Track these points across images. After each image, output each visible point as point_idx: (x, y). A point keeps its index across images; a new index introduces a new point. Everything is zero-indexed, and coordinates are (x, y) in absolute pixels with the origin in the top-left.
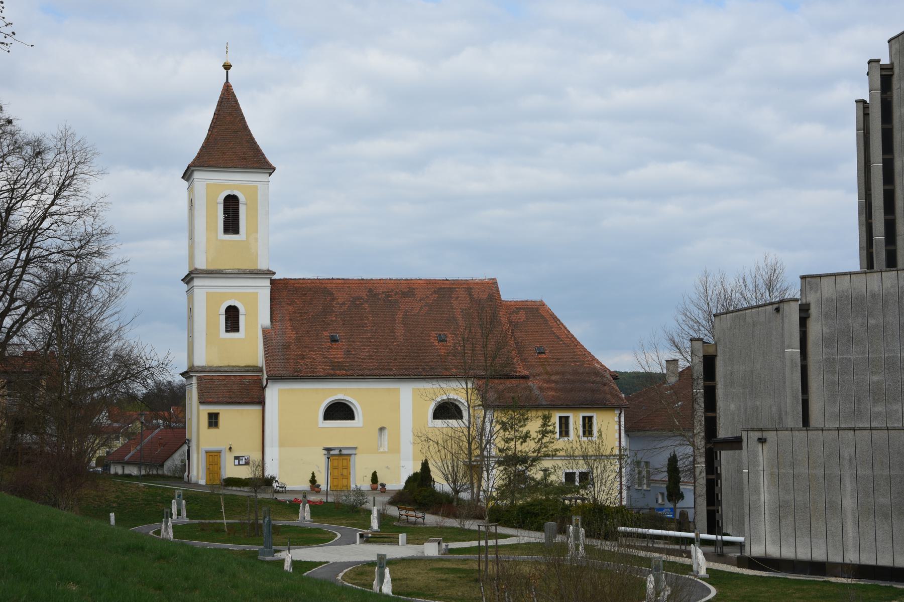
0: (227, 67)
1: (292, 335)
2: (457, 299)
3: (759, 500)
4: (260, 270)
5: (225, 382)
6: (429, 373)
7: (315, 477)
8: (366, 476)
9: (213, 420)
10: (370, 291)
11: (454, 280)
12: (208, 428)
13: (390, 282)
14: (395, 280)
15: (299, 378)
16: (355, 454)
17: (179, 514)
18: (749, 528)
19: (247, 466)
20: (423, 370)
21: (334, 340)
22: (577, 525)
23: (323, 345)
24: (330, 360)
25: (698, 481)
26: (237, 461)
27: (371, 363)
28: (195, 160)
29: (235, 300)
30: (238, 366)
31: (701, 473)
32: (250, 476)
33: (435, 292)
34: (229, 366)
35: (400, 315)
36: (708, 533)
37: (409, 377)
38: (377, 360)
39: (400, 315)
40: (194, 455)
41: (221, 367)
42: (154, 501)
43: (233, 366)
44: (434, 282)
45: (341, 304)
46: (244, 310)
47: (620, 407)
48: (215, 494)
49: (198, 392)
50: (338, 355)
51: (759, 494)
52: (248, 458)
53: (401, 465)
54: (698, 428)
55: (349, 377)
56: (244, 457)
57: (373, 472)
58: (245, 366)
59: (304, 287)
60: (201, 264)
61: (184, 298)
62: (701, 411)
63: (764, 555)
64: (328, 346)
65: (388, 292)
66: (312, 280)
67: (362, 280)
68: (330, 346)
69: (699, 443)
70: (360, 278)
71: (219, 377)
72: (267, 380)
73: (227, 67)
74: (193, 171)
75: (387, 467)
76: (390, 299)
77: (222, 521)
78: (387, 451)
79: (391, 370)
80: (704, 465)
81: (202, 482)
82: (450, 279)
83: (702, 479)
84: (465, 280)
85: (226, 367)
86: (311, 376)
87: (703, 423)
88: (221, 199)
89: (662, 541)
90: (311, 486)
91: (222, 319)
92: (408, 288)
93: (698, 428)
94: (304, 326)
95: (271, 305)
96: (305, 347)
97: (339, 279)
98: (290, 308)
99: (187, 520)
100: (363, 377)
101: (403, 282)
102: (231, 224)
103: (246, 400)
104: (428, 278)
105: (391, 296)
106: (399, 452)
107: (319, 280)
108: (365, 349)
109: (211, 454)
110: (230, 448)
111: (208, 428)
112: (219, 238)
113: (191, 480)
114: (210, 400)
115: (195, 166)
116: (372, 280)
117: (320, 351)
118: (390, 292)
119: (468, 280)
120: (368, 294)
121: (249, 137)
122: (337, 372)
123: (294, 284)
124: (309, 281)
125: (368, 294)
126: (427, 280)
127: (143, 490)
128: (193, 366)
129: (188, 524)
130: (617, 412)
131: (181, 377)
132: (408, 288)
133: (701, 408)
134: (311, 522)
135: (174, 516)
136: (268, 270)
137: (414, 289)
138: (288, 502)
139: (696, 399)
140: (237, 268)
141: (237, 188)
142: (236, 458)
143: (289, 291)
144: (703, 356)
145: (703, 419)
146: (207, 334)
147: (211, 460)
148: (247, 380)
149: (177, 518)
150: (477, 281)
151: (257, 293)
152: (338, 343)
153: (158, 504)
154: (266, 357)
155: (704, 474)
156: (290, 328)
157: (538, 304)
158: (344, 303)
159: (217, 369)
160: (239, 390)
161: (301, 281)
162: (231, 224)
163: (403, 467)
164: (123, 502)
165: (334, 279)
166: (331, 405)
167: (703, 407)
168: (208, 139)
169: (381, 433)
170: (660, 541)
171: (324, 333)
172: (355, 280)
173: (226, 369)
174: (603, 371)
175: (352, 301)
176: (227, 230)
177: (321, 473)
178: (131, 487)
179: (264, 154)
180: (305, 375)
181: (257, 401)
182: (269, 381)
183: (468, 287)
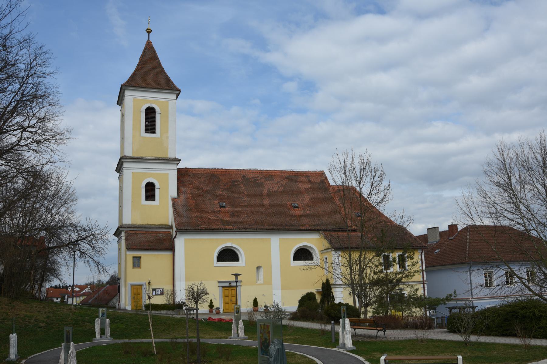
0: (149, 31)
1: (192, 203)
2: (301, 182)
4: (170, 158)
5: (145, 235)
6: (290, 228)
7: (212, 303)
8: (249, 302)
10: (244, 176)
11: (297, 171)
12: (133, 268)
13: (256, 171)
14: (259, 170)
15: (200, 230)
16: (241, 286)
17: (103, 333)
19: (161, 296)
20: (286, 226)
23: (215, 209)
24: (221, 219)
26: (155, 292)
27: (249, 221)
28: (126, 83)
29: (152, 178)
30: (154, 225)
32: (165, 302)
33: (286, 178)
34: (148, 224)
35: (265, 191)
37: (277, 230)
39: (265, 191)
40: (123, 288)
41: (142, 225)
42: (82, 321)
43: (151, 225)
44: (285, 172)
45: (225, 184)
46: (159, 185)
47: (422, 248)
48: (138, 314)
49: (126, 242)
50: (226, 216)
52: (162, 290)
53: (273, 293)
55: (235, 230)
56: (159, 289)
57: (254, 298)
58: (160, 225)
59: (199, 173)
60: (129, 153)
61: (117, 183)
64: (218, 210)
65: (255, 177)
66: (204, 169)
68: (219, 210)
70: (236, 169)
71: (141, 232)
72: (176, 232)
73: (149, 31)
74: (125, 90)
75: (263, 295)
76: (257, 181)
77: (149, 340)
78: (263, 283)
79: (264, 226)
81: (129, 308)
82: (295, 170)
84: (304, 172)
85: (146, 225)
86: (208, 229)
88: (144, 109)
90: (209, 310)
91: (143, 191)
92: (268, 175)
94: (200, 197)
95: (177, 183)
96: (202, 210)
97: (223, 169)
98: (191, 186)
99: (111, 340)
100: (245, 230)
101: (265, 172)
102: (150, 127)
103: (160, 247)
104: (280, 170)
105: (258, 180)
106: (272, 284)
107: (209, 169)
108: (244, 212)
110: (149, 283)
111: (133, 268)
112: (141, 136)
113: (120, 307)
114: (135, 247)
115: (125, 86)
116: (244, 170)
117: (213, 213)
118: (257, 177)
119: (306, 172)
120: (242, 178)
121: (162, 72)
122: (227, 227)
123: (192, 171)
124: (203, 170)
125: (242, 178)
126: (280, 171)
127: (75, 311)
128: (122, 224)
129: (112, 345)
130: (420, 252)
132: (268, 175)
134: (246, 339)
135: (98, 336)
136: (176, 158)
137: (272, 176)
138: (297, 312)
140: (153, 156)
142: (154, 290)
143: (189, 175)
146: (132, 202)
147: (135, 292)
148: (161, 234)
149: (101, 337)
150: (312, 172)
151: (168, 174)
152: (225, 208)
153: (86, 323)
154: (174, 216)
156: (191, 198)
158: (227, 184)
159: (139, 226)
160: (156, 241)
161: (198, 170)
162: (150, 127)
163: (274, 294)
164: (52, 322)
165: (219, 169)
166: (222, 250)
168: (135, 72)
169: (258, 270)
171: (215, 202)
172: (233, 170)
173: (146, 226)
175: (232, 182)
177: (216, 300)
178: (63, 308)
179: (173, 82)
180: (204, 228)
181: (169, 248)
182: (178, 232)
183: (307, 175)
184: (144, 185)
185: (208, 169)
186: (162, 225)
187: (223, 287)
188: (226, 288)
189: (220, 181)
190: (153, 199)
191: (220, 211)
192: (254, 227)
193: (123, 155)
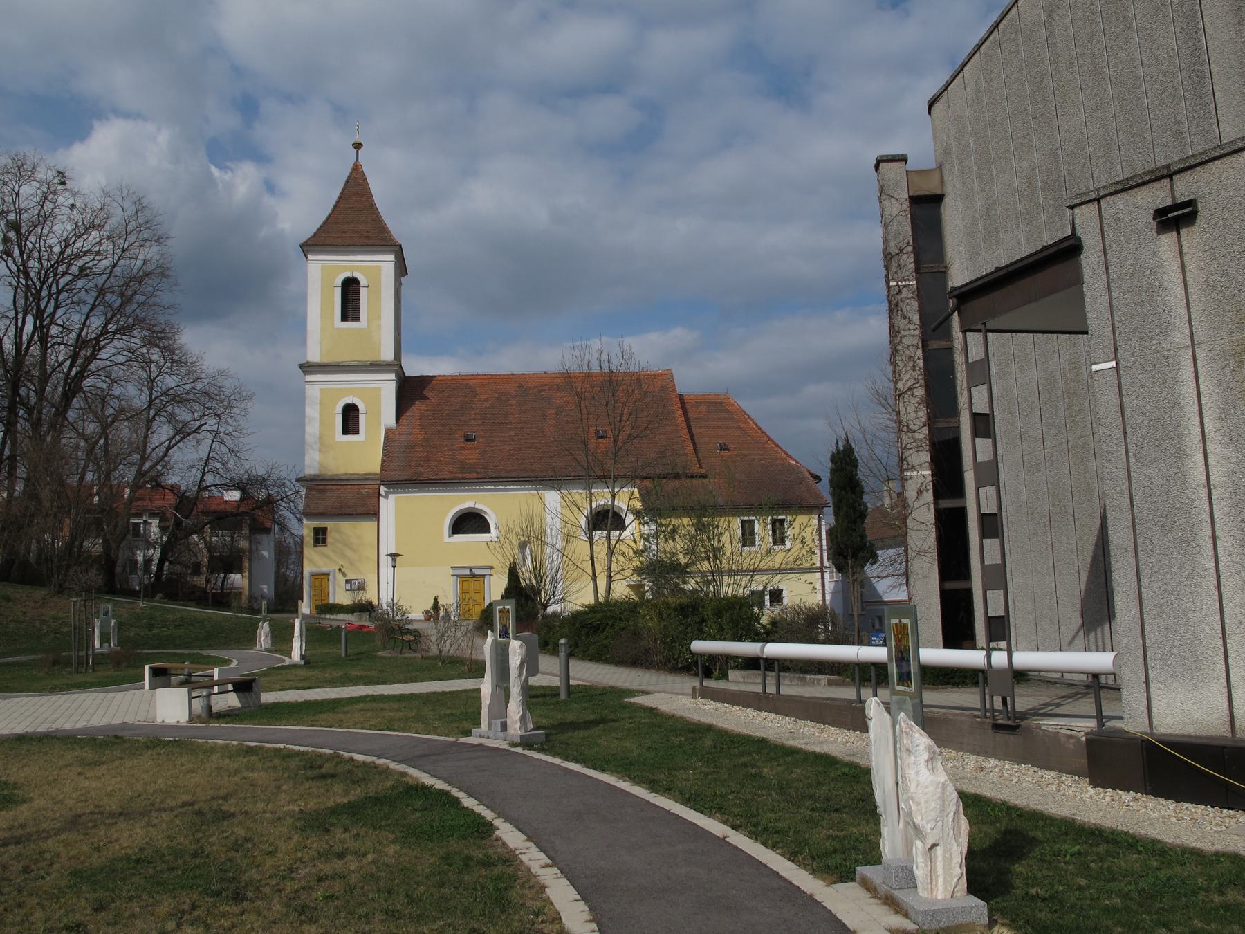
0: (358, 146)
3: (1181, 479)
9: (320, 537)
10: (520, 385)
18: (1135, 610)
21: (469, 439)
22: (504, 633)
25: (913, 515)
31: (920, 492)
34: (346, 474)
36: (947, 645)
38: (518, 461)
43: (350, 474)
51: (1179, 453)
54: (907, 377)
58: (366, 474)
62: (912, 332)
63: (1224, 731)
67: (513, 374)
69: (912, 416)
73: (358, 146)
80: (929, 472)
83: (924, 509)
85: (343, 475)
87: (920, 363)
88: (339, 281)
89: (824, 679)
93: (907, 377)
109: (317, 577)
122: (467, 475)
131: (628, 590)
133: (912, 327)
139: (897, 305)
141: (358, 269)
144: (910, 197)
145: (920, 352)
155: (929, 496)
157: (722, 397)
158: (486, 400)
167: (918, 322)
170: (820, 677)
174: (798, 467)
176: (345, 318)
184: (339, 408)
185: (460, 375)
186: (370, 474)
187: (458, 576)
188: (464, 579)
189: (475, 397)
190: (355, 431)
191: (464, 448)
192: (515, 474)
193: (305, 361)
